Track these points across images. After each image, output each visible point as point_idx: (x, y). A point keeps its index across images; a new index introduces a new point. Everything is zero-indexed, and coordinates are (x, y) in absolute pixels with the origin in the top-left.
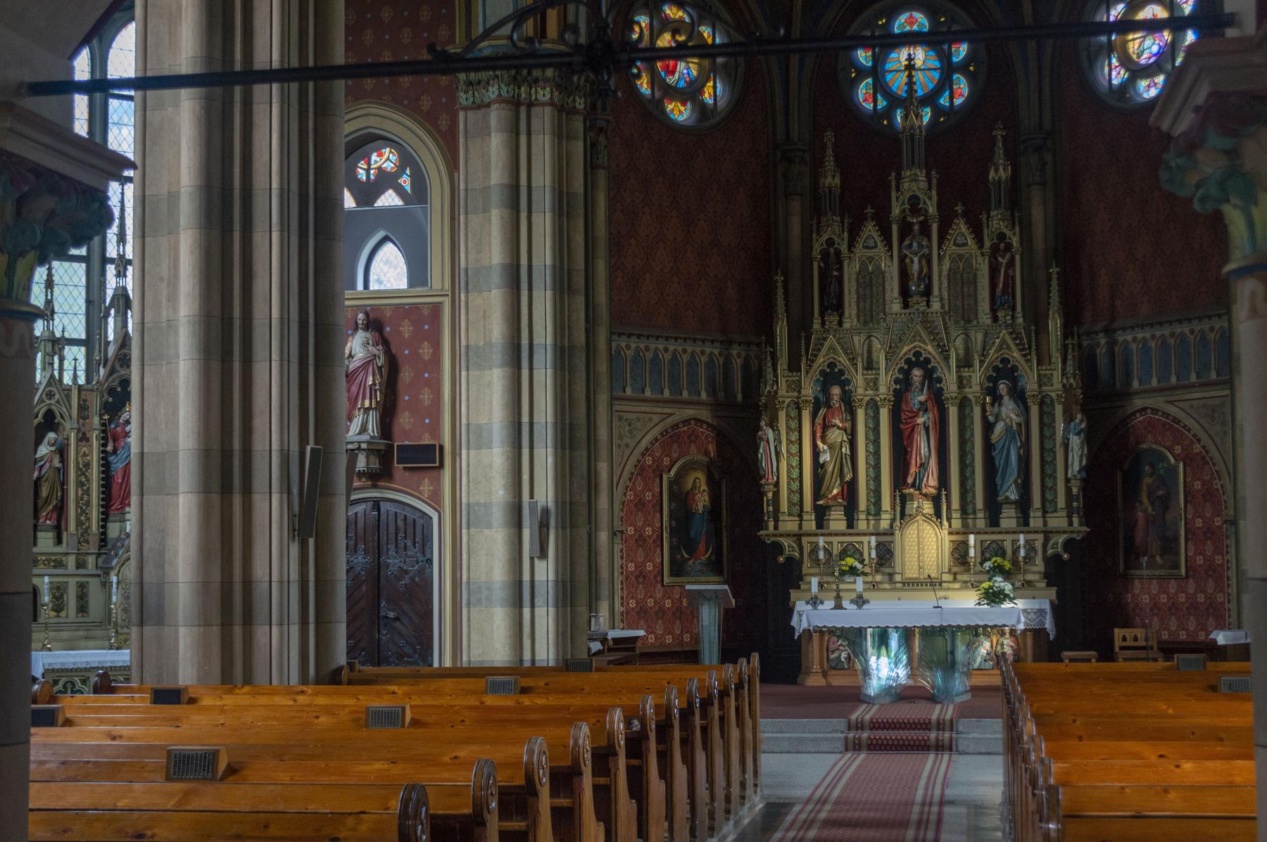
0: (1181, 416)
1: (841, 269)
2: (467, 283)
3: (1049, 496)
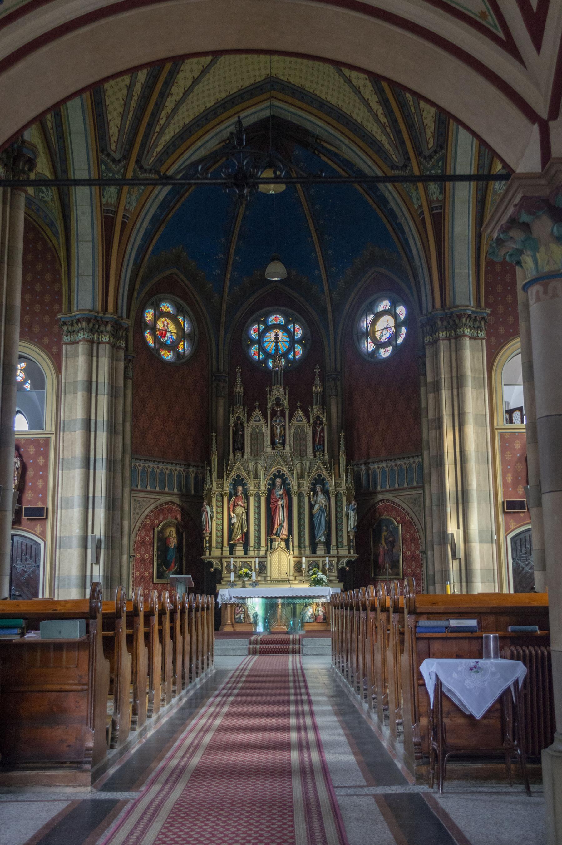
0: (400, 502)
1: (243, 431)
2: (64, 427)
3: (340, 540)
